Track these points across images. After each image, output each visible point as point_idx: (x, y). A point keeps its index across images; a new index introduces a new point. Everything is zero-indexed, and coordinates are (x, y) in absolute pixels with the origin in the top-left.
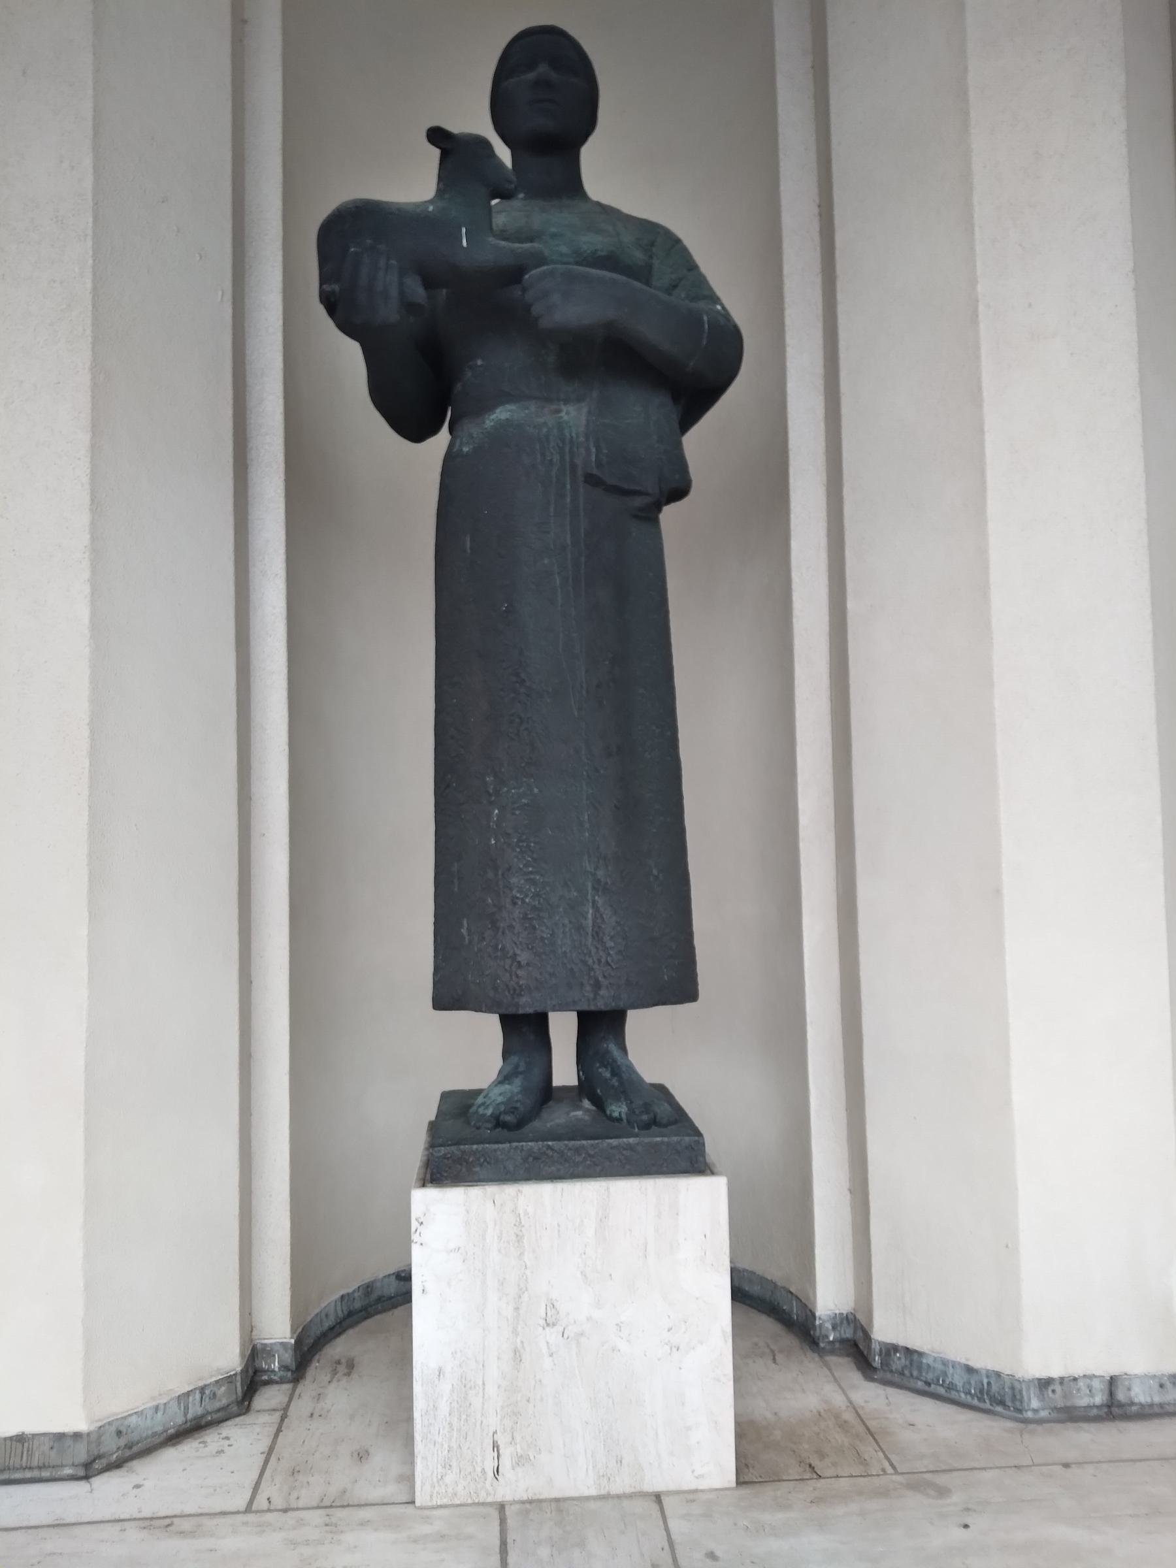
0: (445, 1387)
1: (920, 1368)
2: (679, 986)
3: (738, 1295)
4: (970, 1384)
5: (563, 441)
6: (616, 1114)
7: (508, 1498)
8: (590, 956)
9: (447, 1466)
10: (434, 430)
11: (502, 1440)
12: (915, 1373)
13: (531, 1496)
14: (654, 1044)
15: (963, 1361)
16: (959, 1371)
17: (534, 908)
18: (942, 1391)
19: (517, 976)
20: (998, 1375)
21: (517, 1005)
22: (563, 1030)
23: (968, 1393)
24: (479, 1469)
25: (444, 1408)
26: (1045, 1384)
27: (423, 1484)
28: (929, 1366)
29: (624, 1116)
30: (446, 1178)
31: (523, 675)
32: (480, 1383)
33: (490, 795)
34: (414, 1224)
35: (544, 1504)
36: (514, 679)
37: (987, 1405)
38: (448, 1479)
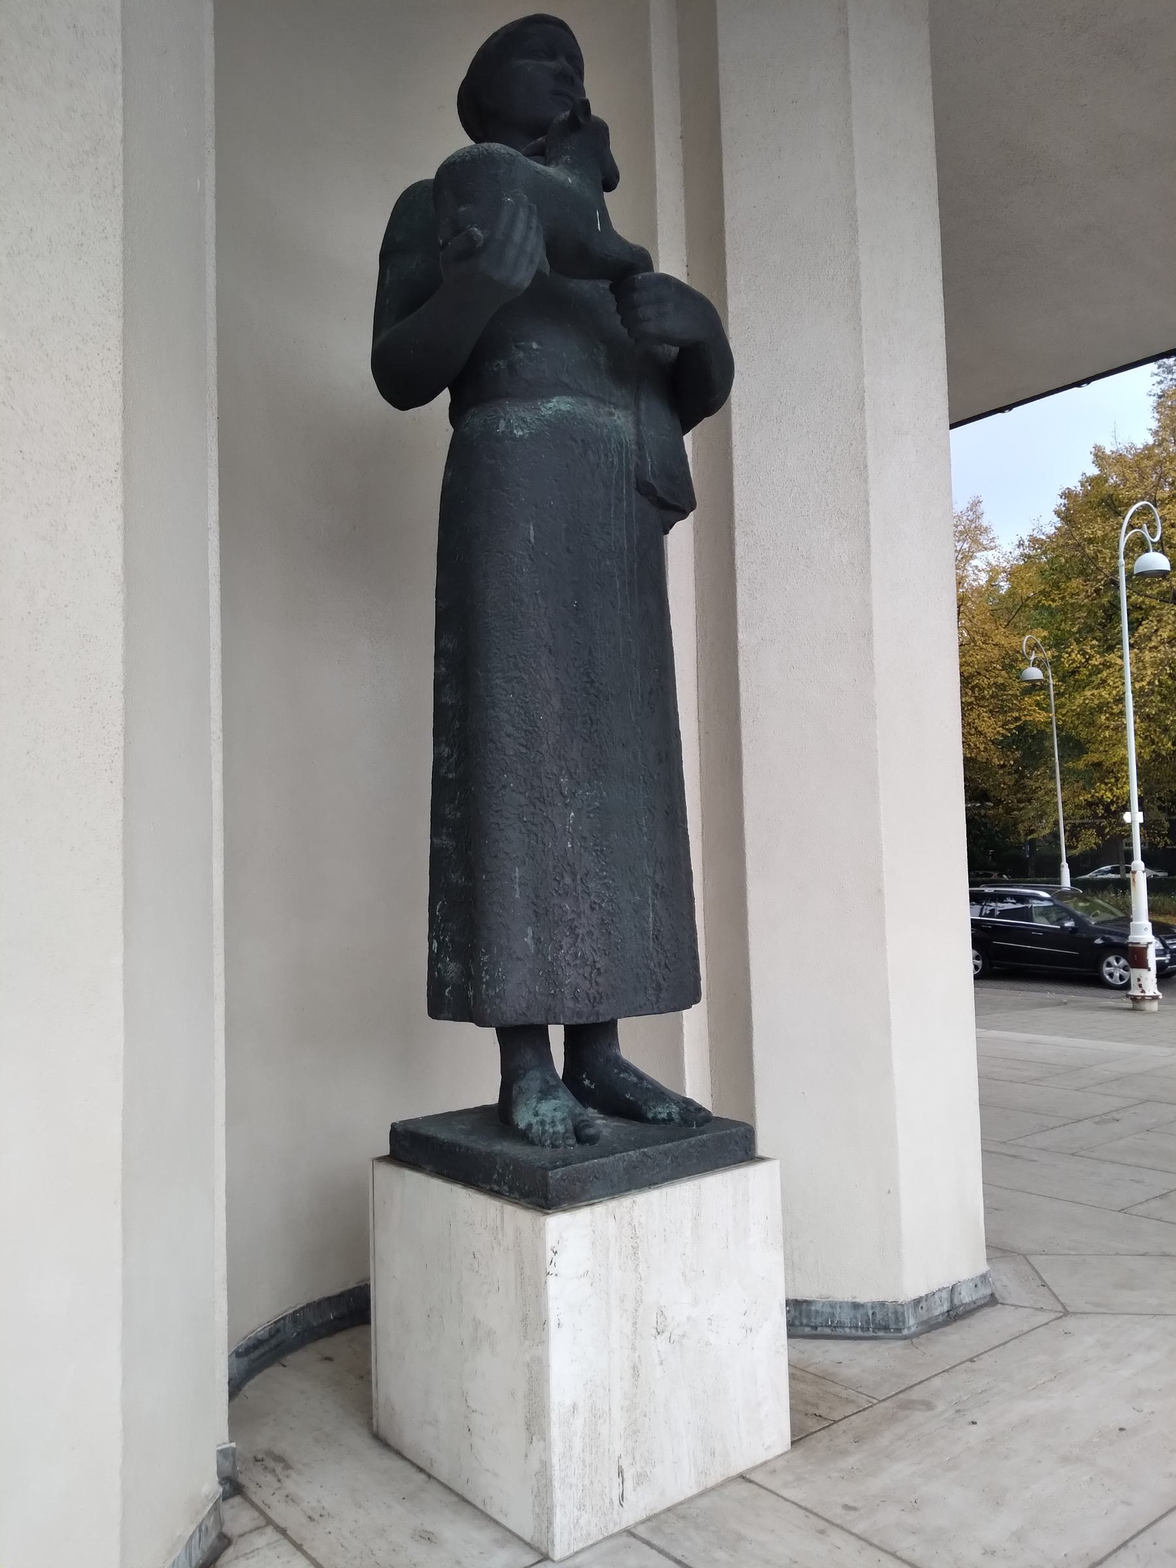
0: (578, 1424)
1: (809, 1316)
3: (988, 1247)
4: (855, 1318)
5: (621, 446)
6: (664, 1115)
7: (632, 1522)
8: (652, 959)
9: (581, 1507)
11: (625, 1464)
12: (805, 1321)
13: (649, 1513)
15: (850, 1300)
16: (846, 1309)
17: (609, 913)
18: (828, 1331)
19: (597, 984)
20: (883, 1304)
21: (598, 1014)
23: (856, 1327)
24: (607, 1501)
25: (578, 1444)
26: (917, 1302)
27: (562, 1534)
28: (817, 1312)
29: (675, 1116)
31: (592, 676)
32: (607, 1409)
33: (565, 797)
35: (662, 1516)
36: (585, 679)
37: (871, 1334)
38: (582, 1522)
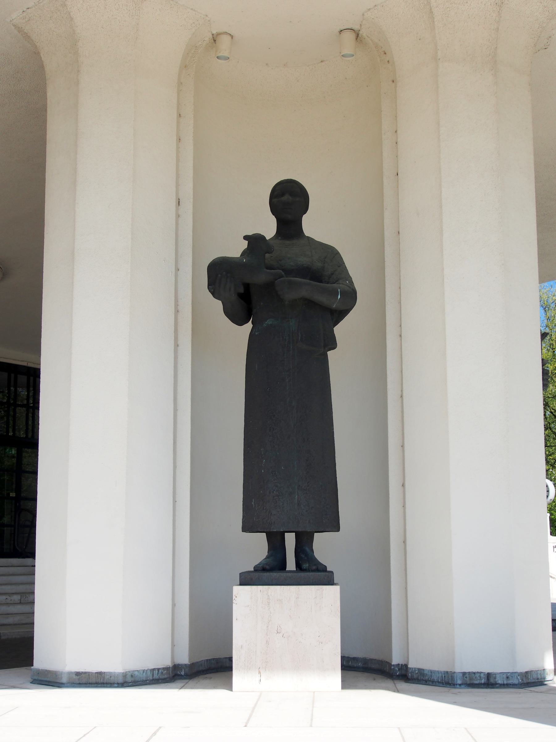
2: (333, 524)
10: (247, 322)
14: (324, 546)
20: (447, 672)
22: (290, 540)
30: (18, 489)
34: (234, 597)
